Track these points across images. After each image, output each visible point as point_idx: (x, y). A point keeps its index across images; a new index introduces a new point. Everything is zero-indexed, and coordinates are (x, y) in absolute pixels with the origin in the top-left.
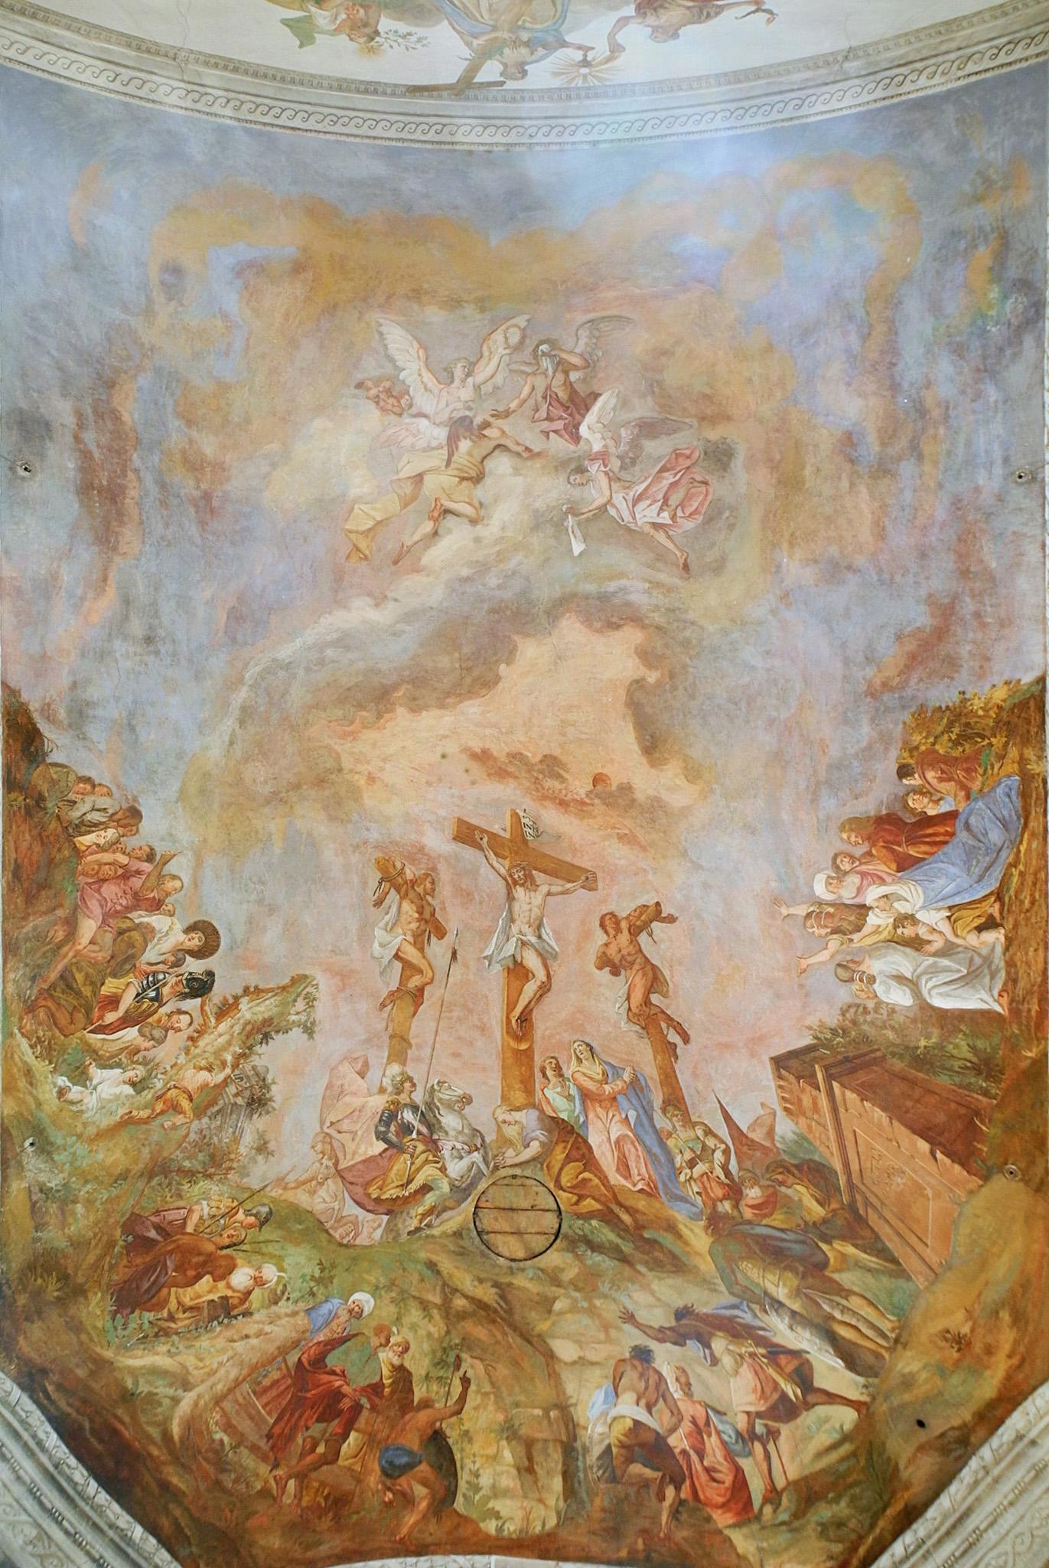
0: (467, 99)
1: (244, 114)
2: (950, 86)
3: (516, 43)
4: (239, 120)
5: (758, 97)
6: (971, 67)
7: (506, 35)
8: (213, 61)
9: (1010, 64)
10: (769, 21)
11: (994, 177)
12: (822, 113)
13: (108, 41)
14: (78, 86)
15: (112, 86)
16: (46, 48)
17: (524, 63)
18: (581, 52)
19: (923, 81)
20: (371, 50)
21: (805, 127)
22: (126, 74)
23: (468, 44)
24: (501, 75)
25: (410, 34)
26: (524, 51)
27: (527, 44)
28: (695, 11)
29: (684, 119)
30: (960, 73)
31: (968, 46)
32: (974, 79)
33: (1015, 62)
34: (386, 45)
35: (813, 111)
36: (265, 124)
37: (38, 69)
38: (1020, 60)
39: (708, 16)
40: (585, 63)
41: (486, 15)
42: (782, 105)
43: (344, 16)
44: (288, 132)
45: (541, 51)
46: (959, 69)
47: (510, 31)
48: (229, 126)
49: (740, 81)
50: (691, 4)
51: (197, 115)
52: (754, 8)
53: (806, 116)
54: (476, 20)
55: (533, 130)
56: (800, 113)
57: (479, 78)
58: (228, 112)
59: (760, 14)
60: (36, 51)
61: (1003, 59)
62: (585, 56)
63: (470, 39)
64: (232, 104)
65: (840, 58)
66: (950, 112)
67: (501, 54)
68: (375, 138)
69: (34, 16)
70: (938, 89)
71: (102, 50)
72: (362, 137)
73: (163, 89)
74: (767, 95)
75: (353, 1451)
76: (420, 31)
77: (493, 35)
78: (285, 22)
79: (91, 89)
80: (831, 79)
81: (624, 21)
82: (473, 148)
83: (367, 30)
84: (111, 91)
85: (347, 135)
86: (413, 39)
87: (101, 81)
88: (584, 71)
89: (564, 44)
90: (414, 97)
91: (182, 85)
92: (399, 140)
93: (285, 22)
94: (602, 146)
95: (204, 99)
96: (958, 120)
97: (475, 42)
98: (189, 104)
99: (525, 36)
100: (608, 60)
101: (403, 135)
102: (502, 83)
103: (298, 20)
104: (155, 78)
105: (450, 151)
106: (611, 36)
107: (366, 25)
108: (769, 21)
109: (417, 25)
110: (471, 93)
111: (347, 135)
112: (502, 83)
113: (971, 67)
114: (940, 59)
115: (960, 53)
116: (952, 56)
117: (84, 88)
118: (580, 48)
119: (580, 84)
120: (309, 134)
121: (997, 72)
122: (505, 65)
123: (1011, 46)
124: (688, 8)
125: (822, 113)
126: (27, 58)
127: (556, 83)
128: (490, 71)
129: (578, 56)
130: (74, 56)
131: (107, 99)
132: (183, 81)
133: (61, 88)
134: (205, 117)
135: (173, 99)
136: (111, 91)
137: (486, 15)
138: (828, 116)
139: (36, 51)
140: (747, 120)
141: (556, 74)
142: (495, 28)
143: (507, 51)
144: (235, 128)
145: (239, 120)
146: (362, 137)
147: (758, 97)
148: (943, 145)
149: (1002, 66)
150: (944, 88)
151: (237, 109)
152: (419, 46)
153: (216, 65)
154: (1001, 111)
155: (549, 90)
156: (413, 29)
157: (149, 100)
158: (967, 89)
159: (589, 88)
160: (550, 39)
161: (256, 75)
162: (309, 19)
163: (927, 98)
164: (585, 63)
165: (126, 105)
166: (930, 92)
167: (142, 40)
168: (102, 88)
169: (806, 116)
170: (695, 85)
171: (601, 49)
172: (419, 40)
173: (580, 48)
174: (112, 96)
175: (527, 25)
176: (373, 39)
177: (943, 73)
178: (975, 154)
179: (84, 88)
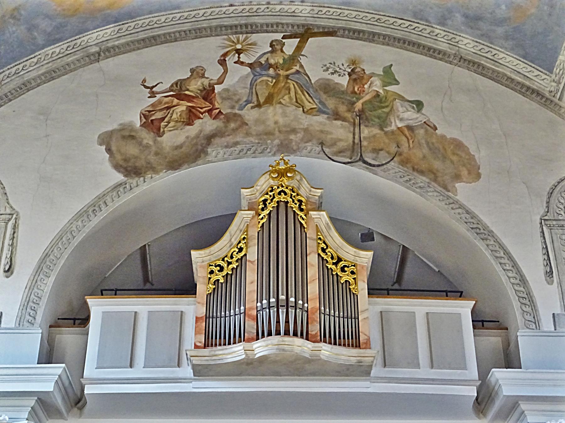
0: (303, 26)
1: (429, 29)
2: (43, 51)
3: (276, 67)
4: (432, 27)
5: (142, 31)
6: (35, 60)
7: (282, 72)
8: (440, 56)
9: (16, 65)
10: (144, 81)
11: (11, 20)
12: (107, 29)
13: (494, 71)
14: (515, 56)
15: (497, 52)
16: (526, 74)
17: (271, 52)
18: (241, 60)
19: (57, 50)
20: (353, 62)
21: (115, 22)
22: (489, 55)
23: (301, 66)
24: (284, 44)
25: (332, 74)
26: (272, 61)
27: (271, 66)
28: (183, 89)
29: (181, 18)
30: (39, 57)
31: (38, 67)
32: (32, 56)
33: (14, 67)
34: (345, 66)
35: (112, 29)
36: (418, 23)
37: (533, 67)
38: (11, 68)
39: (176, 84)
40: (239, 52)
41: (292, 86)
42: (129, 29)
43: (366, 86)
44: (405, 18)
45: (263, 60)
46: (40, 58)
47: (278, 75)
48: (438, 25)
49: (153, 37)
50: (187, 92)
51: (455, 32)
52: (154, 89)
53: (115, 26)
54: (297, 82)
55: (267, 10)
56: (119, 27)
57: (295, 42)
58: (437, 31)
59: (151, 85)
60: (533, 74)
61: (20, 67)
62: (239, 57)
63: (301, 70)
64: (435, 34)
65: (102, 54)
66: (40, 40)
67: (284, 59)
68: (357, 11)
69: (528, 88)
70: (49, 48)
71: (498, 67)
72: (364, 12)
73: (471, 46)
74: (137, 32)
75: (384, 112)
76: (327, 75)
77: (288, 73)
78: (397, 83)
79: (508, 53)
80: (104, 43)
81: (220, 82)
82: (301, 4)
83: (354, 76)
84: (498, 50)
85: (372, 13)
86: (331, 70)
87: (502, 55)
88: (239, 47)
89: (250, 65)
90: (333, 27)
91: (460, 46)
92: (343, 9)
93: (397, 83)
94: (227, 4)
95: (449, 38)
96: (35, 39)
97: (297, 68)
98: (458, 38)
99: (271, 71)
100: (225, 55)
101: (340, 11)
102: (284, 38)
103: (390, 84)
104: (474, 51)
105: (314, 3)
106: (226, 71)
107: (355, 80)
108: (144, 81)
109: (328, 80)
110: (301, 30)
111: (372, 13)
112: (284, 38)
113: (35, 60)
114: (50, 60)
115: (41, 64)
116: (45, 62)
117: (512, 55)
118: (242, 63)
119: (241, 36)
120: (394, 16)
121: (22, 61)
122: (282, 51)
123: (17, 72)
124: (188, 90)
125: (107, 29)
126: (537, 73)
127: (254, 37)
128: (290, 45)
129: (243, 58)
130: (513, 68)
131: (501, 47)
132: (459, 47)
133: (524, 58)
134: (450, 31)
135: (466, 41)
136: (498, 50)
137: (292, 86)
138: (104, 28)
139: (533, 74)
140: (147, 21)
141: (254, 44)
142: (287, 77)
143: (281, 61)
144: (435, 24)
145: (432, 27)
146: (364, 12)
147: (142, 31)
148: (40, 27)
149: (19, 64)
150: (46, 49)
151: (433, 32)
152: (328, 65)
153: (440, 52)
154: (15, 47)
155: (258, 32)
156: (330, 77)
157: (479, 43)
158: (34, 52)
159: (236, 33)
160: (258, 69)
161: (419, 45)
162: (385, 84)
163: (54, 44)
164: (239, 52)
165: (491, 43)
166: (52, 47)
167: (475, 72)
168: (503, 52)
169: (115, 26)
170: (178, 35)
171: (231, 61)
172: (327, 69)
173: (242, 63)
174: (498, 48)
175: (270, 79)
176: (352, 70)
177: (48, 55)
178: (22, 27)
179: (512, 55)
